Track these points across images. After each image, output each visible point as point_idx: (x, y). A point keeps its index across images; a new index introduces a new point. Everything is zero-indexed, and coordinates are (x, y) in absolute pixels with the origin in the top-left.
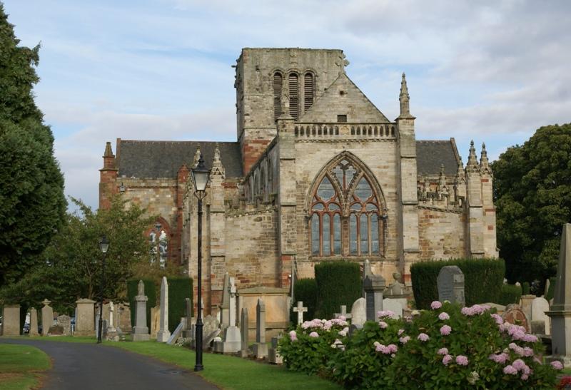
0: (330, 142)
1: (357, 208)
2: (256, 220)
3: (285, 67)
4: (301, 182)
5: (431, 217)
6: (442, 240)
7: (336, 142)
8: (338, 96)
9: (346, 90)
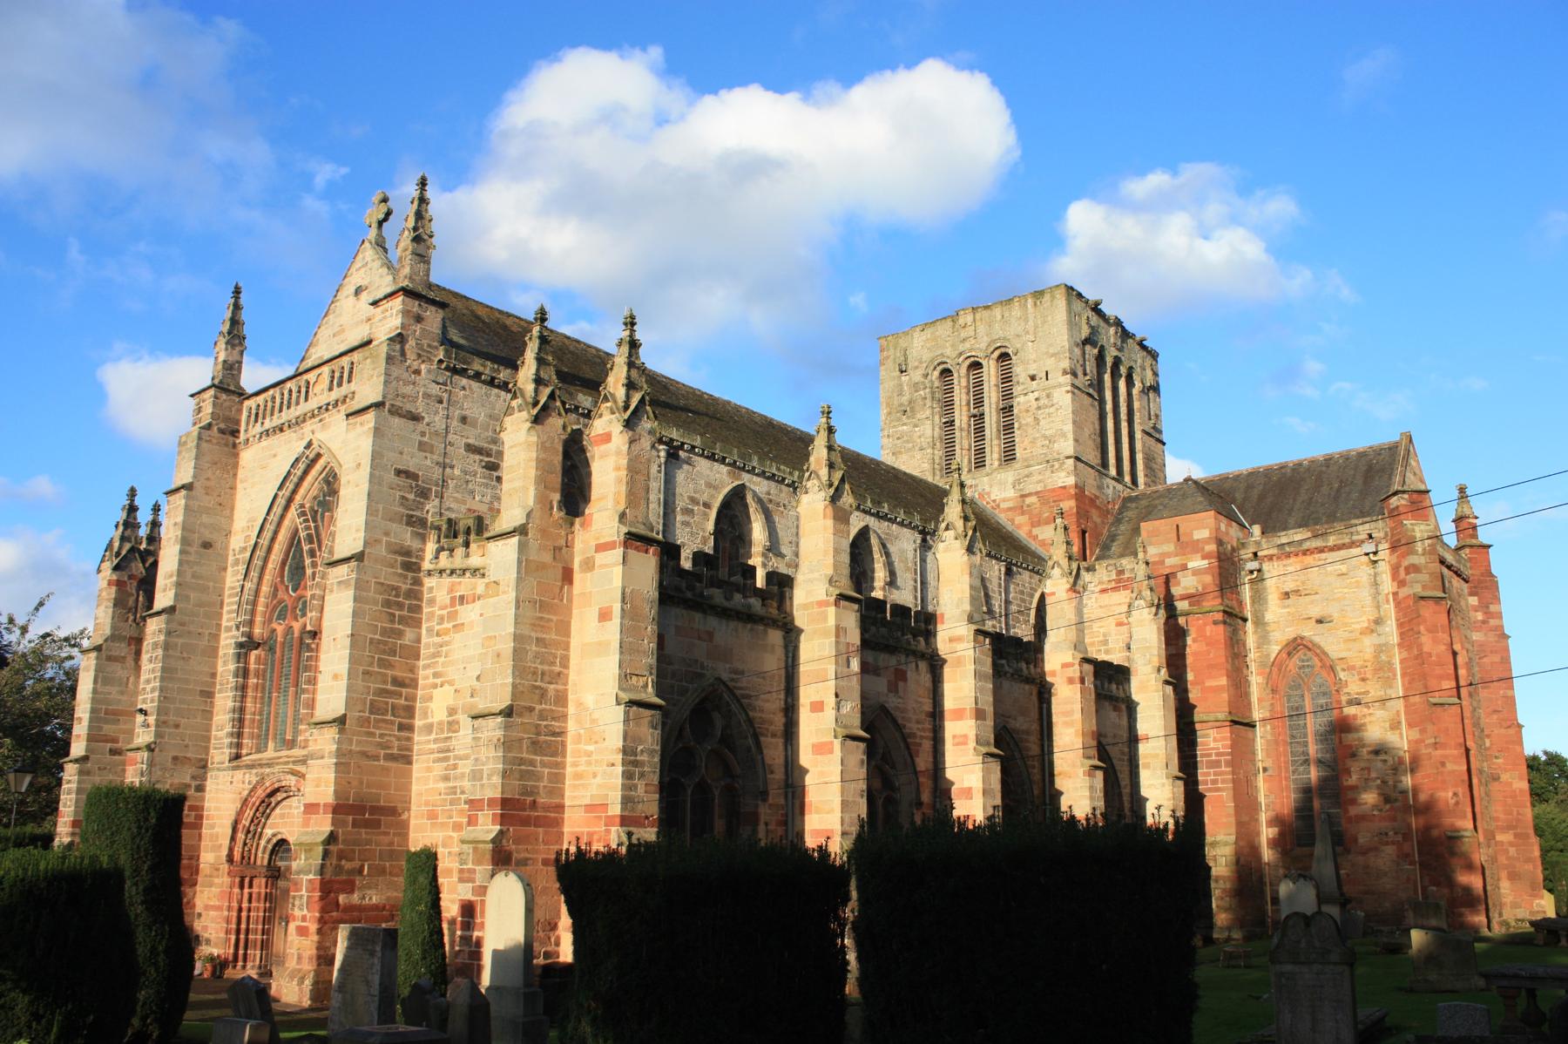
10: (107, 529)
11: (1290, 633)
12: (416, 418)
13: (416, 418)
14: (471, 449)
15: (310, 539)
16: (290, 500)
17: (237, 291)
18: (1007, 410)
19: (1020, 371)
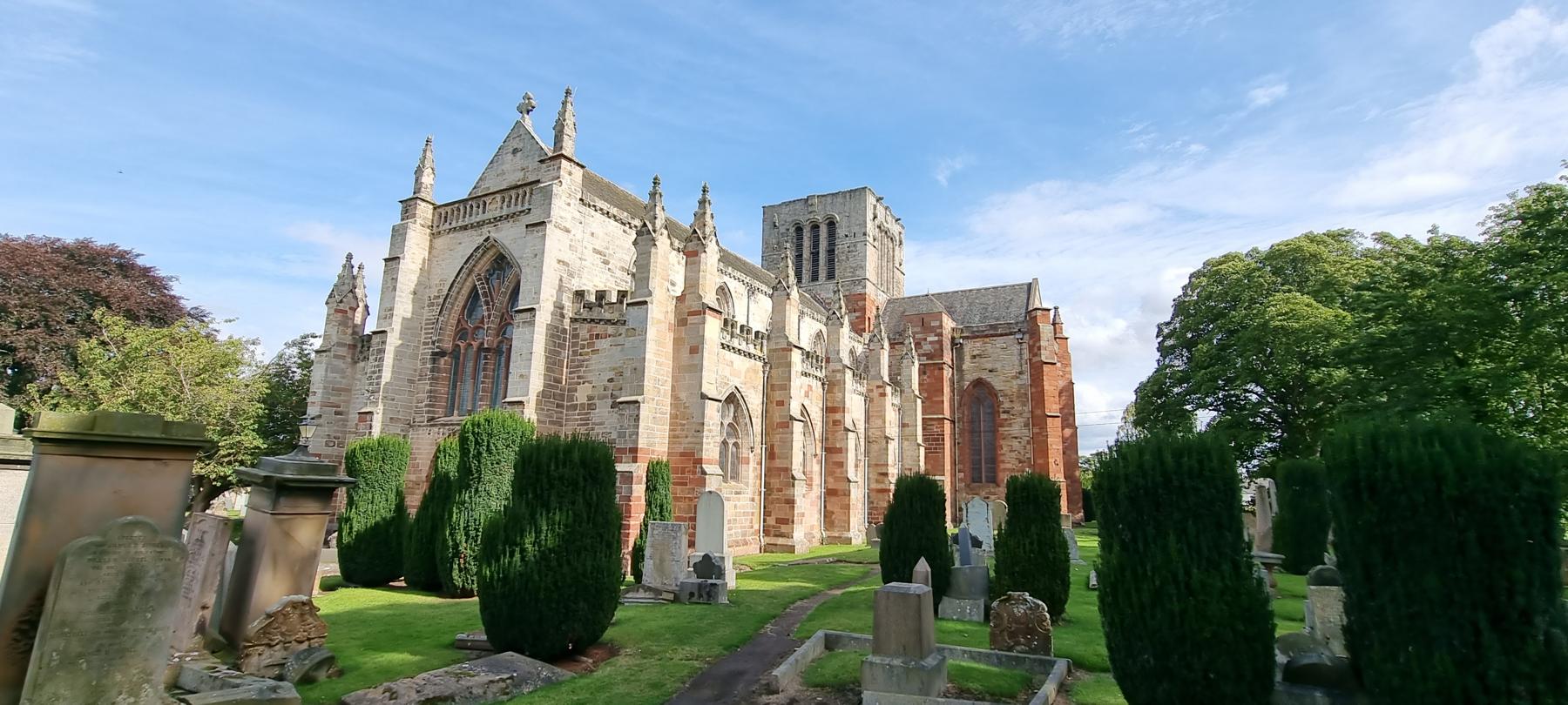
0: (472, 226)
3: (803, 219)
6: (610, 380)
8: (510, 156)
9: (520, 146)
10: (334, 271)
11: (975, 376)
12: (568, 231)
13: (568, 231)
14: (596, 251)
15: (485, 294)
16: (471, 271)
18: (831, 252)
19: (841, 232)
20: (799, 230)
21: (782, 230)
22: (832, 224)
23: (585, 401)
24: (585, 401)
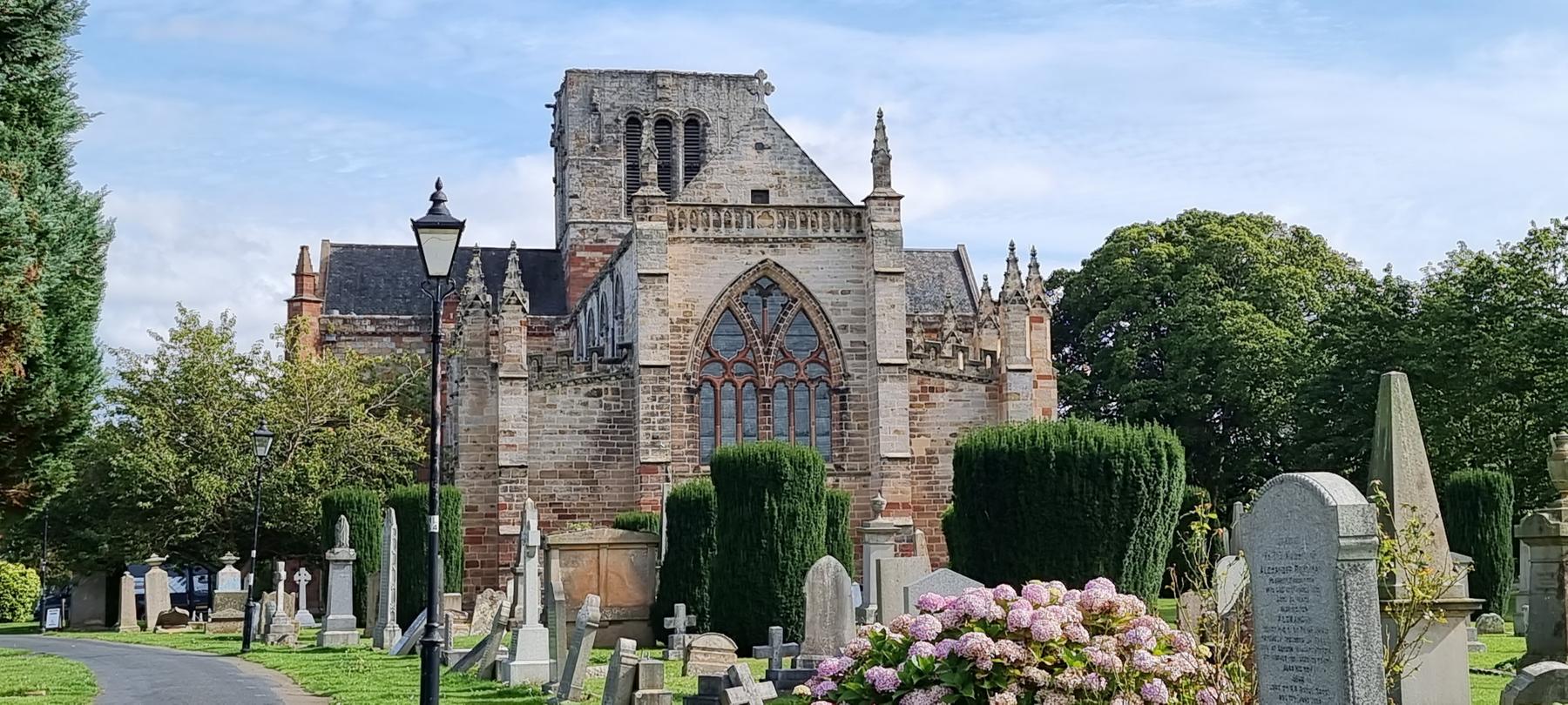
0: (736, 241)
1: (788, 371)
2: (589, 395)
4: (679, 321)
5: (932, 389)
7: (747, 241)
9: (768, 142)
17: (880, 115)
20: (634, 122)
21: (608, 119)
22: (694, 123)
23: (924, 454)
24: (924, 454)
